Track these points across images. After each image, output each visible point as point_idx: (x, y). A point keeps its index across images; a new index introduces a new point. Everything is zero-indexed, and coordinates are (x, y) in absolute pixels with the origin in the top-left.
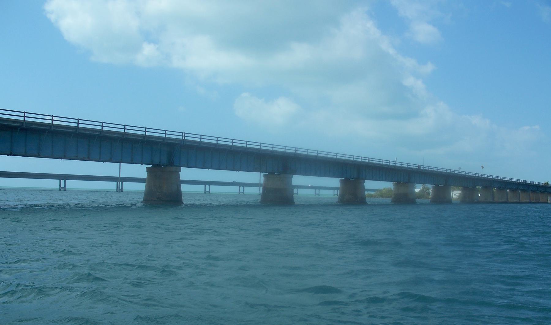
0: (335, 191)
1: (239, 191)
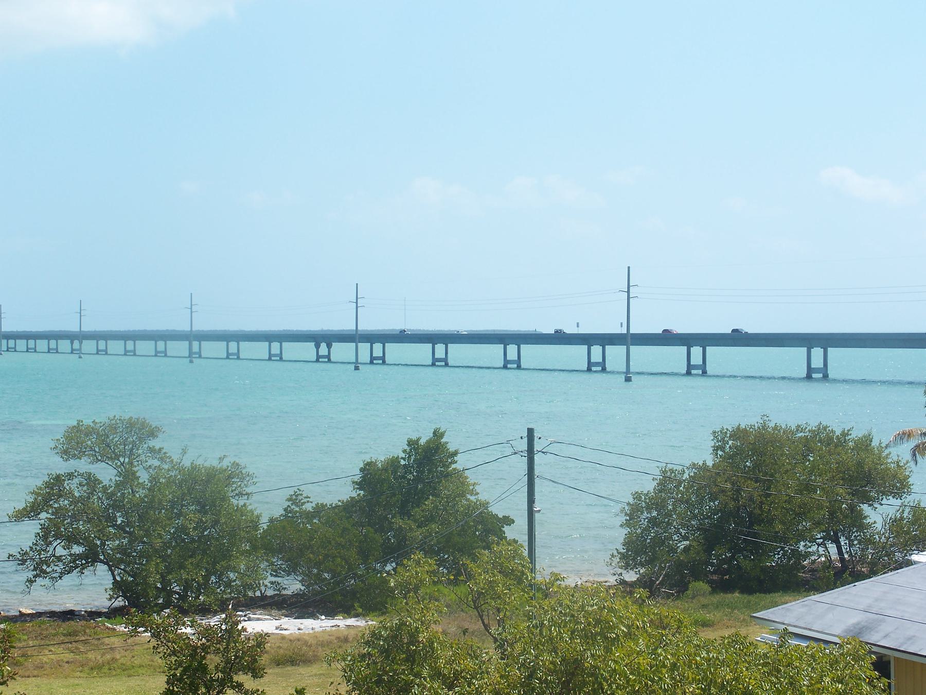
0: (10, 341)
1: (125, 348)
